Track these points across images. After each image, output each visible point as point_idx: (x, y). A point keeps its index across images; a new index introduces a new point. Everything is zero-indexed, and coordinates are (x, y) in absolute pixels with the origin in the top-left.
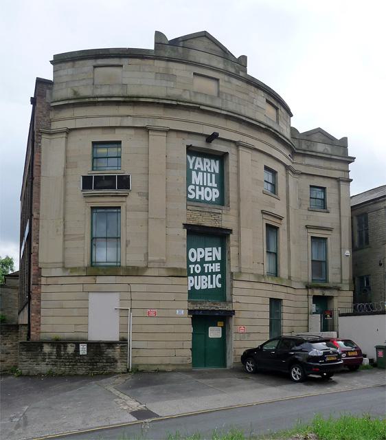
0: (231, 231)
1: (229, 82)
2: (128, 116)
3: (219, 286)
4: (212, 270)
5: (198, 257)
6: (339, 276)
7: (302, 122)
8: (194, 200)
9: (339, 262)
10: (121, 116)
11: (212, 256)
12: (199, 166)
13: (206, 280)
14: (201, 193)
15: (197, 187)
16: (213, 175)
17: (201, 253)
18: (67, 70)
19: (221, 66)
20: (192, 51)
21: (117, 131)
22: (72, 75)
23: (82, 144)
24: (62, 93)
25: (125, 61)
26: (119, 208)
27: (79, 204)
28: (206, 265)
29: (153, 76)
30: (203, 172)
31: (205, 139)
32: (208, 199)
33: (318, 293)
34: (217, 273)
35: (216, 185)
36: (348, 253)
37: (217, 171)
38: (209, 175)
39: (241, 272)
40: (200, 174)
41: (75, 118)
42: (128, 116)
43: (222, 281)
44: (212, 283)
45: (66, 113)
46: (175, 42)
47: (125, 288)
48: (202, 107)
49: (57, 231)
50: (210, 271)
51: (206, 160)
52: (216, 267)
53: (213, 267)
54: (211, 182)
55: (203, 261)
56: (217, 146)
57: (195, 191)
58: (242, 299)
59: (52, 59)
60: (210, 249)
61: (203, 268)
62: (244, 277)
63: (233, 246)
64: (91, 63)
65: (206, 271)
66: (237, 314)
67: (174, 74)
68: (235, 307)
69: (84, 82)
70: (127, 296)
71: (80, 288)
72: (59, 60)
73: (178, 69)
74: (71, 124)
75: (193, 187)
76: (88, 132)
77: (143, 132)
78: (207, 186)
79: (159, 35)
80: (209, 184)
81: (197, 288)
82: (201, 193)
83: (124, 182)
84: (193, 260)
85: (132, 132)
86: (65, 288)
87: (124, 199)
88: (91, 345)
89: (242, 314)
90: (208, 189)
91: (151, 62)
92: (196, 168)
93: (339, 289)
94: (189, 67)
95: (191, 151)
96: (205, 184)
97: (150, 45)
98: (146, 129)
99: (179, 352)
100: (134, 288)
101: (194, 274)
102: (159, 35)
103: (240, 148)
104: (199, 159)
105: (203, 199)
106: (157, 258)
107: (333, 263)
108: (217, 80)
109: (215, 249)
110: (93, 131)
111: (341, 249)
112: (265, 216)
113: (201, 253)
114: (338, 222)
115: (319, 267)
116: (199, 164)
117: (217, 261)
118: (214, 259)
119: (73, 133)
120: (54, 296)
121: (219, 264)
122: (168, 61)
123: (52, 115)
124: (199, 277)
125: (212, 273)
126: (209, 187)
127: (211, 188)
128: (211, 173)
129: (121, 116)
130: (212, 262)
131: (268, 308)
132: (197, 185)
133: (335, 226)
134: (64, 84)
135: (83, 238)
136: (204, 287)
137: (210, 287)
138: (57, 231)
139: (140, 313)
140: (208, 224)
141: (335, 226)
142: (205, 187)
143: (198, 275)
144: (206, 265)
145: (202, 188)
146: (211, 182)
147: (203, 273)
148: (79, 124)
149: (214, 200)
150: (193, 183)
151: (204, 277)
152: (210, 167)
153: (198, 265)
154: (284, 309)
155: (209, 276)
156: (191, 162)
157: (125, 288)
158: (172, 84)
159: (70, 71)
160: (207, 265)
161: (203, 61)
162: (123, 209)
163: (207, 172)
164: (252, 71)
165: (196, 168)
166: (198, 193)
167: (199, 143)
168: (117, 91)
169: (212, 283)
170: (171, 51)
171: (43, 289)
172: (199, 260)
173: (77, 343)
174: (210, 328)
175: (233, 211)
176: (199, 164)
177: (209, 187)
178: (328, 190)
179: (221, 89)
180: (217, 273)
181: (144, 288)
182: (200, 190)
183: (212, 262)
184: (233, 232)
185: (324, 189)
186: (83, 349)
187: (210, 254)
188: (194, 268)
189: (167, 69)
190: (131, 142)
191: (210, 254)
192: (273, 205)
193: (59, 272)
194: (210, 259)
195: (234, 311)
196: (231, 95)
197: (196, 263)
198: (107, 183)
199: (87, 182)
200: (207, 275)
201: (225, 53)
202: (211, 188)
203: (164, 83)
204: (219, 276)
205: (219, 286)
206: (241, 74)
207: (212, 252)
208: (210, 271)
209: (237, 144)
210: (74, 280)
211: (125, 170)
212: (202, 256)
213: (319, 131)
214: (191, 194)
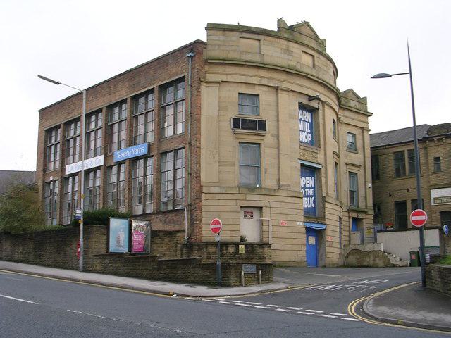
2: (265, 77)
6: (364, 203)
7: (342, 85)
9: (364, 192)
10: (261, 77)
18: (219, 36)
20: (298, 35)
21: (257, 87)
22: (224, 41)
23: (232, 93)
25: (261, 37)
26: (259, 144)
27: (229, 138)
32: (208, 261)
33: (355, 215)
34: (312, 196)
35: (309, 131)
36: (370, 185)
41: (227, 74)
42: (265, 77)
45: (220, 69)
46: (291, 28)
49: (214, 158)
51: (304, 112)
56: (314, 104)
64: (238, 34)
72: (211, 28)
73: (295, 48)
74: (224, 78)
76: (235, 85)
77: (273, 90)
79: (280, 21)
83: (262, 126)
85: (266, 89)
86: (221, 202)
87: (262, 138)
88: (247, 245)
91: (278, 40)
93: (366, 213)
97: (273, 27)
98: (277, 89)
99: (299, 253)
100: (273, 204)
102: (280, 21)
106: (285, 183)
107: (361, 192)
108: (313, 56)
110: (240, 85)
111: (365, 182)
114: (362, 158)
115: (352, 194)
120: (212, 209)
123: (207, 68)
127: (308, 133)
129: (261, 77)
133: (362, 164)
134: (217, 47)
138: (214, 158)
139: (276, 223)
141: (362, 164)
147: (305, 196)
148: (230, 78)
159: (222, 38)
161: (307, 42)
162: (262, 146)
164: (329, 51)
166: (301, 136)
167: (305, 101)
168: (257, 58)
171: (204, 202)
173: (237, 245)
178: (357, 136)
179: (316, 63)
180: (312, 196)
181: (279, 205)
183: (309, 188)
185: (354, 135)
186: (242, 249)
189: (288, 46)
190: (266, 97)
193: (216, 190)
198: (251, 125)
199: (236, 123)
202: (308, 133)
203: (286, 57)
205: (313, 206)
210: (229, 197)
211: (263, 117)
212: (304, 183)
213: (351, 91)
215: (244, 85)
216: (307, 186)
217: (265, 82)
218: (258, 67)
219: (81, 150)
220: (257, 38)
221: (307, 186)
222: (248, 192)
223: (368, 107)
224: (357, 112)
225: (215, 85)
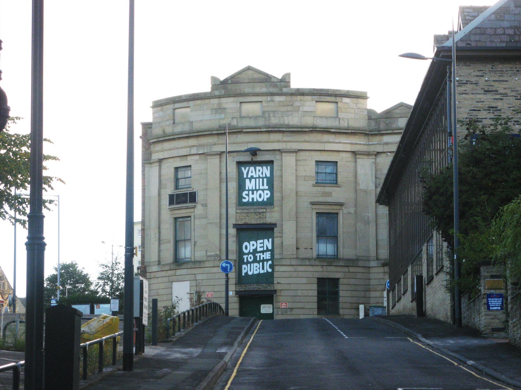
0: (275, 225)
1: (272, 101)
3: (270, 270)
4: (263, 258)
5: (251, 248)
8: (248, 204)
11: (263, 247)
12: (252, 174)
13: (258, 267)
14: (254, 196)
15: (251, 192)
16: (265, 180)
17: (253, 245)
19: (264, 90)
20: (249, 66)
21: (189, 158)
24: (157, 131)
25: (191, 103)
26: (190, 217)
28: (258, 255)
29: (209, 112)
30: (256, 178)
31: (249, 153)
32: (260, 200)
34: (267, 260)
35: (267, 187)
37: (268, 175)
38: (261, 180)
39: (337, 258)
40: (253, 180)
43: (271, 266)
44: (263, 269)
47: (192, 277)
48: (244, 130)
50: (262, 259)
51: (258, 168)
52: (267, 255)
53: (264, 256)
54: (263, 185)
55: (255, 251)
57: (248, 195)
58: (282, 281)
59: (151, 105)
60: (262, 241)
61: (255, 257)
62: (284, 262)
63: (277, 237)
64: (171, 107)
65: (258, 259)
66: (278, 294)
67: (224, 107)
68: (277, 287)
69: (168, 123)
70: (194, 282)
71: (166, 279)
75: (246, 192)
78: (259, 189)
80: (261, 187)
81: (250, 273)
82: (254, 196)
84: (246, 251)
85: (197, 157)
86: (160, 280)
87: (192, 210)
89: (283, 293)
90: (260, 192)
92: (249, 176)
94: (235, 99)
95: (240, 164)
96: (257, 188)
100: (199, 277)
101: (248, 263)
103: (283, 154)
104: (252, 168)
105: (255, 200)
109: (266, 241)
112: (314, 207)
113: (253, 245)
116: (252, 172)
117: (268, 250)
118: (265, 249)
119: (164, 162)
121: (270, 253)
122: (219, 98)
124: (252, 265)
125: (263, 261)
126: (261, 190)
127: (263, 190)
128: (263, 178)
130: (263, 252)
131: (315, 287)
132: (250, 190)
135: (170, 241)
136: (255, 273)
137: (262, 272)
140: (253, 222)
142: (257, 190)
143: (250, 263)
144: (258, 255)
145: (255, 192)
146: (263, 185)
147: (255, 261)
149: (265, 200)
150: (247, 188)
151: (256, 264)
152: (262, 173)
153: (250, 255)
154: (341, 287)
155: (261, 263)
156: (245, 172)
157: (192, 277)
158: (223, 116)
160: (259, 254)
161: (247, 90)
162: (192, 217)
163: (259, 177)
165: (249, 176)
166: (251, 196)
167: (247, 158)
169: (263, 269)
170: (227, 88)
172: (251, 251)
174: (262, 306)
175: (276, 209)
176: (252, 172)
177: (261, 190)
180: (267, 260)
182: (253, 194)
183: (263, 252)
184: (278, 225)
187: (262, 245)
188: (247, 258)
189: (219, 104)
191: (262, 245)
192: (329, 194)
194: (262, 249)
195: (276, 290)
196: (274, 112)
197: (249, 253)
198: (183, 199)
200: (259, 262)
201: (267, 79)
202: (263, 190)
203: (218, 116)
204: (270, 262)
205: (270, 270)
206: (285, 90)
207: (263, 243)
208: (262, 259)
209: (280, 151)
210: (163, 274)
212: (254, 247)
214: (245, 198)
215: (178, 159)
216: (259, 249)
217: (194, 151)
218: (187, 137)
219: (450, 109)
220: (187, 106)
221: (259, 249)
222: (177, 268)
223: (25, 134)
224: (258, 132)
225: (291, 154)
